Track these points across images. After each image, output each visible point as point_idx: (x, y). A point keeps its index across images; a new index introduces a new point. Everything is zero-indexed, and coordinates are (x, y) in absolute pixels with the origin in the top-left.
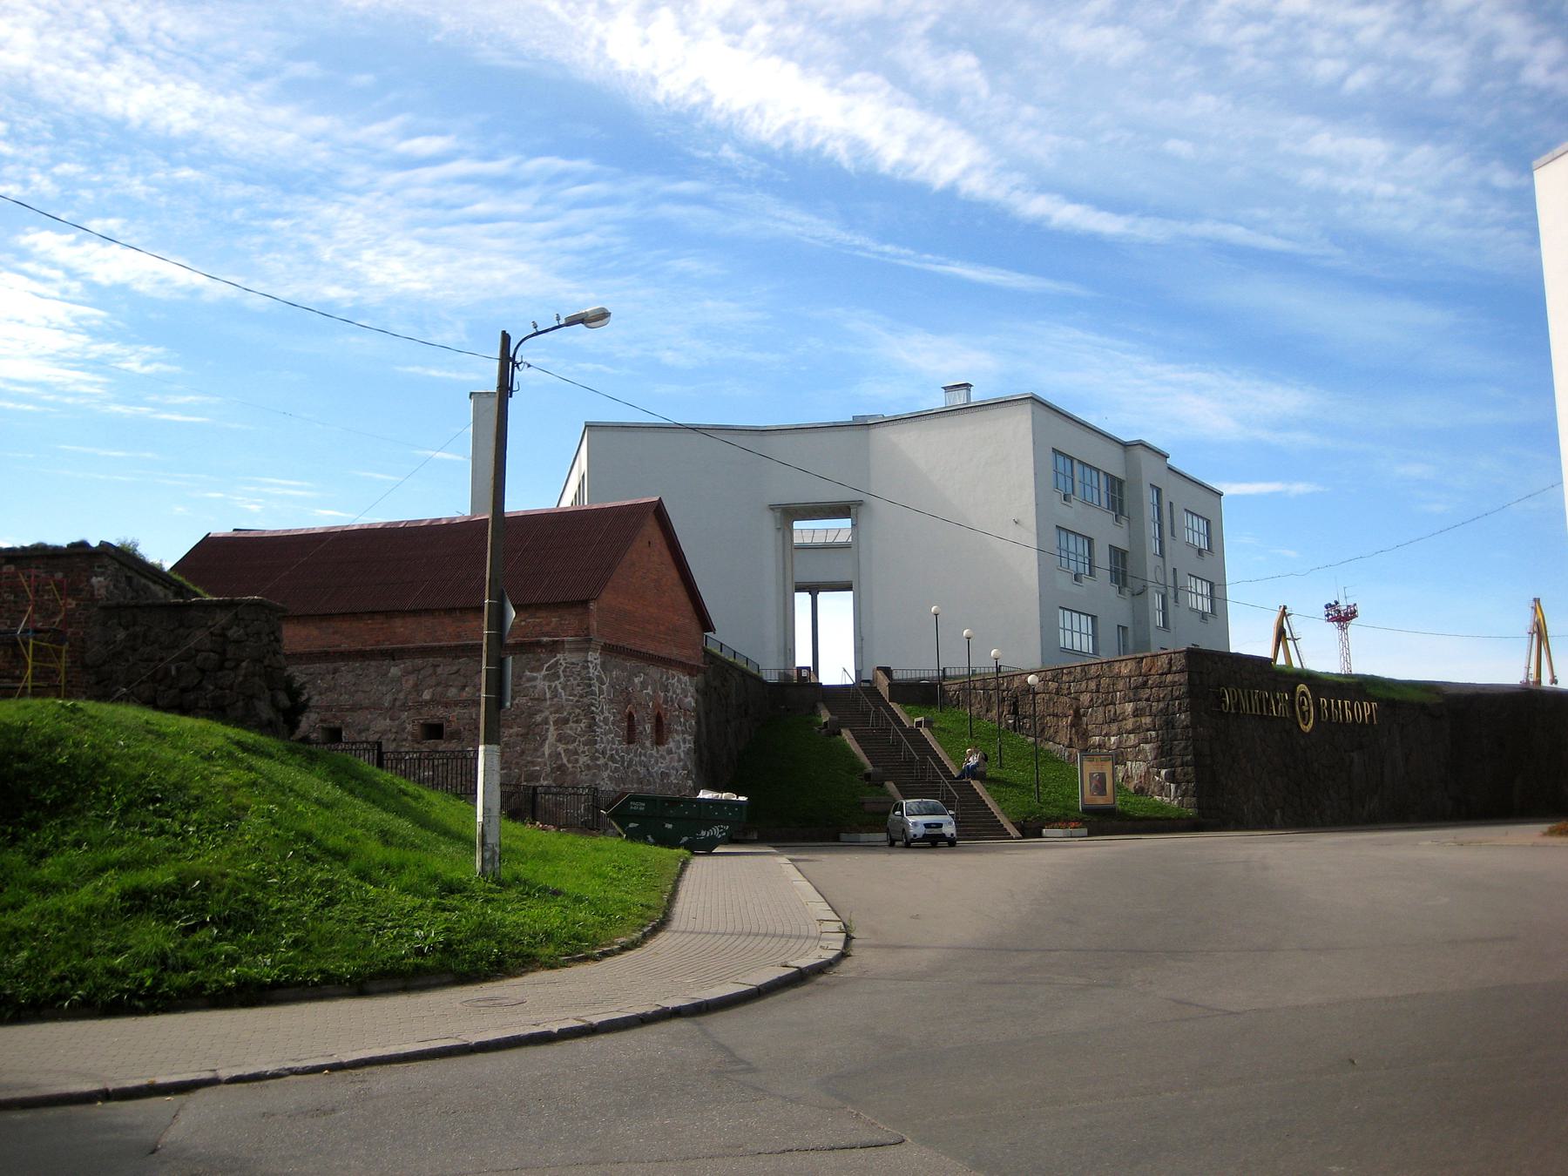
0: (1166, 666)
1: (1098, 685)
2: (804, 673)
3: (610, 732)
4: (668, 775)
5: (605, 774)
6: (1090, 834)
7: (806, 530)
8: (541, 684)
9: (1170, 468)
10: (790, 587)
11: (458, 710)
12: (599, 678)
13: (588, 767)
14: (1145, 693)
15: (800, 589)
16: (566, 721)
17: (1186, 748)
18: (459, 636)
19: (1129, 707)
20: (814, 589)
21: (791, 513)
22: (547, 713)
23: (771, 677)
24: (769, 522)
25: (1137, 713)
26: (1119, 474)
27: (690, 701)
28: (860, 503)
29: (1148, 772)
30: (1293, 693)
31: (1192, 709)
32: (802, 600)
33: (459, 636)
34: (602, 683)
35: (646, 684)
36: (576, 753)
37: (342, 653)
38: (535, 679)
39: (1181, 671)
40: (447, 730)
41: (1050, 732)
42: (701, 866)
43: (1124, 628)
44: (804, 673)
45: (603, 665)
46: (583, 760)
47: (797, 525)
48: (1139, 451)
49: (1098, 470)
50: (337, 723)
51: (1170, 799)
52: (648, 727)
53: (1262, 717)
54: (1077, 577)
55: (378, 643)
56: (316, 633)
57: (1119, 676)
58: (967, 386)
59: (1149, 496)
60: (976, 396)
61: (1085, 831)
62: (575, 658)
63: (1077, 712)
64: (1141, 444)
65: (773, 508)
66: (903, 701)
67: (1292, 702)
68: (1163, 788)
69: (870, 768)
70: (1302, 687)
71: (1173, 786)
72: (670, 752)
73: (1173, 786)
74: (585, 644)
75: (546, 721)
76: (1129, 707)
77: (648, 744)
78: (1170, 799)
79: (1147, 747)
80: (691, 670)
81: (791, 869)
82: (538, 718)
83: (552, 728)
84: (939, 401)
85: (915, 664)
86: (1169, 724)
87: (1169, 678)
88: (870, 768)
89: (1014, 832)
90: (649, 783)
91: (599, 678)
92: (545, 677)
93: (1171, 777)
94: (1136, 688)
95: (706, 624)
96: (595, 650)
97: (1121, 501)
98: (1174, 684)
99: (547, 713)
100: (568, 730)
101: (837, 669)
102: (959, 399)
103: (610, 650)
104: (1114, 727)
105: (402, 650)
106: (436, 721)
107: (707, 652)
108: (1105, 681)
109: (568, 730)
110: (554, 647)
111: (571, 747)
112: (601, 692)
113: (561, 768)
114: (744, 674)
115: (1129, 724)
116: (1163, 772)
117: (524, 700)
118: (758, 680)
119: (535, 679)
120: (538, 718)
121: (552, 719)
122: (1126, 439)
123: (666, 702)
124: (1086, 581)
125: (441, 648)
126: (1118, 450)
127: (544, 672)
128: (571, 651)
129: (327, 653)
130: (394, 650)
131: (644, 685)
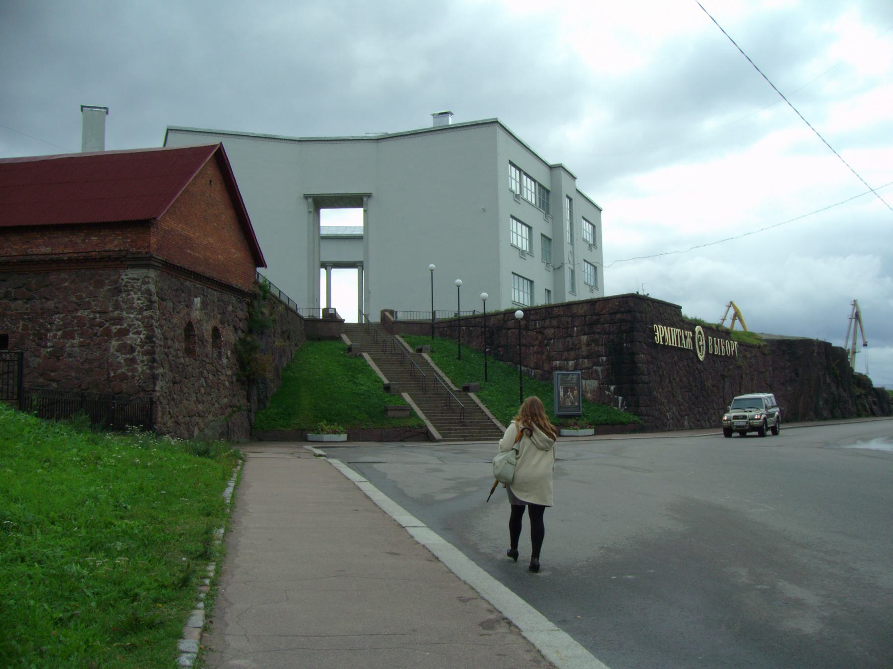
7: (336, 220)
10: (317, 264)
15: (324, 265)
19: (584, 338)
20: (328, 266)
21: (321, 202)
23: (304, 313)
24: (304, 208)
26: (547, 185)
28: (369, 196)
30: (694, 332)
32: (323, 271)
42: (543, 303)
43: (549, 292)
47: (323, 212)
57: (574, 316)
60: (451, 121)
61: (344, 437)
65: (306, 197)
67: (693, 339)
70: (698, 328)
71: (620, 398)
73: (620, 398)
79: (599, 369)
84: (428, 123)
85: (413, 307)
87: (619, 316)
93: (618, 392)
95: (258, 260)
96: (155, 268)
97: (548, 204)
101: (349, 314)
102: (442, 122)
104: (572, 354)
107: (256, 283)
114: (287, 308)
115: (584, 350)
116: (612, 388)
118: (295, 313)
122: (551, 162)
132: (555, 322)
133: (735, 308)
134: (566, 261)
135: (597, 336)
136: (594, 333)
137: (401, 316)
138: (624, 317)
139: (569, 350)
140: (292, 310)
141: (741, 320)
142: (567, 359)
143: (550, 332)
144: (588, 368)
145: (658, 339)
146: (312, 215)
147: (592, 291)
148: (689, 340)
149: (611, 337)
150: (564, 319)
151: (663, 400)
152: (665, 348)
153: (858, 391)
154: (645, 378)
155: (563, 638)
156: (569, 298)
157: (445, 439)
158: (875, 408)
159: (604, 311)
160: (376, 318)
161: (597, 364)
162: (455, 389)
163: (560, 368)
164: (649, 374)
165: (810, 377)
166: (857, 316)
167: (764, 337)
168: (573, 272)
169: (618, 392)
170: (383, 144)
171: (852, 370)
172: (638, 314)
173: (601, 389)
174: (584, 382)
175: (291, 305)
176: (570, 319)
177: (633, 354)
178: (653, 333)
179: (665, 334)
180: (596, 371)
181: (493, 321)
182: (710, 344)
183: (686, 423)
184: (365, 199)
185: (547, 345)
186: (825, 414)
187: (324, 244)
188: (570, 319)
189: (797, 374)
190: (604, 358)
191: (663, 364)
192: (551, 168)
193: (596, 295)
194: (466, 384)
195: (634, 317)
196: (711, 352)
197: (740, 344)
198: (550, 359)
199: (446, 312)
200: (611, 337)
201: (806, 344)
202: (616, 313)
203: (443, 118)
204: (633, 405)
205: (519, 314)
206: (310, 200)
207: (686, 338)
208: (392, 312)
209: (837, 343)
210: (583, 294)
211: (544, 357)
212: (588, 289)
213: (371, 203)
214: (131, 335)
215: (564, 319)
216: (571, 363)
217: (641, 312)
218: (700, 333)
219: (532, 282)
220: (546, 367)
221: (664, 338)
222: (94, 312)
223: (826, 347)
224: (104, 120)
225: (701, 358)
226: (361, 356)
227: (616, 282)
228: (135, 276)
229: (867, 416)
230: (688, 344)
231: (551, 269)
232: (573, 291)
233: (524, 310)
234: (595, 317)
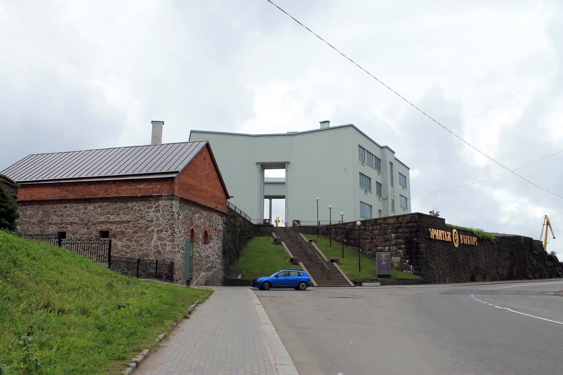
1: (381, 227)
2: (267, 221)
3: (182, 236)
4: (209, 257)
5: (178, 255)
6: (381, 285)
7: (271, 174)
8: (152, 214)
9: (396, 159)
10: (263, 197)
11: (115, 226)
12: (177, 213)
13: (170, 252)
15: (266, 197)
16: (162, 231)
18: (118, 193)
19: (393, 235)
20: (270, 197)
21: (264, 166)
22: (153, 227)
23: (255, 222)
24: (257, 169)
25: (397, 238)
27: (221, 227)
28: (288, 163)
30: (452, 233)
32: (267, 201)
33: (118, 193)
34: (179, 215)
35: (201, 219)
36: (165, 245)
37: (68, 200)
38: (149, 212)
40: (110, 234)
43: (380, 211)
44: (267, 221)
45: (180, 207)
46: (168, 248)
47: (266, 171)
48: (386, 150)
49: (373, 155)
50: (64, 230)
52: (201, 236)
53: (442, 240)
55: (83, 195)
56: (58, 191)
57: (388, 224)
58: (328, 122)
59: (388, 164)
60: (331, 125)
62: (168, 203)
64: (387, 147)
65: (257, 164)
70: (454, 230)
71: (411, 266)
72: (210, 247)
73: (411, 266)
74: (172, 197)
75: (153, 231)
77: (200, 243)
79: (401, 251)
80: (221, 214)
81: (256, 301)
82: (150, 230)
83: (155, 234)
84: (318, 127)
85: (309, 220)
87: (410, 224)
88: (292, 256)
89: (352, 284)
90: (200, 260)
91: (177, 213)
92: (154, 211)
93: (410, 263)
94: (397, 228)
96: (176, 200)
98: (412, 226)
99: (153, 227)
100: (162, 235)
102: (326, 126)
103: (183, 201)
104: (387, 243)
105: (93, 199)
106: (106, 230)
107: (229, 208)
109: (162, 235)
110: (158, 198)
111: (163, 242)
112: (178, 219)
113: (159, 252)
114: (244, 219)
115: (393, 242)
116: (407, 261)
117: (144, 221)
119: (149, 212)
120: (150, 230)
121: (156, 230)
122: (382, 145)
123: (209, 226)
125: (110, 198)
126: (379, 149)
127: (153, 209)
128: (165, 200)
129: (62, 200)
130: (90, 199)
131: (200, 218)
132: (379, 227)
133: (548, 219)
134: (389, 195)
135: (400, 234)
136: (398, 233)
137: (302, 224)
138: (413, 224)
139: (386, 241)
140: (247, 221)
141: (550, 226)
142: (385, 246)
143: (376, 232)
144: (395, 251)
145: (432, 236)
146: (260, 173)
147: (404, 210)
148: (449, 236)
149: (407, 235)
150: (383, 225)
151: (434, 267)
152: (436, 240)
153: (550, 264)
154: (425, 256)
155: (283, 351)
156: (391, 214)
157: (319, 285)
158: (560, 273)
159: (403, 222)
160: (290, 225)
161: (400, 249)
162: (327, 260)
163: (381, 251)
164: (426, 254)
165: (519, 258)
166: (548, 223)
167: (494, 235)
168: (393, 201)
169: (410, 263)
170: (295, 137)
171: (546, 252)
172: (421, 223)
173: (401, 262)
174: (393, 258)
175: (248, 218)
176: (386, 226)
177: (417, 244)
178: (429, 233)
179: (437, 234)
180: (399, 252)
181: (348, 226)
182: (461, 238)
183: (448, 280)
184: (286, 165)
185: (375, 238)
186: (530, 276)
187: (266, 186)
188: (386, 226)
189: (512, 255)
190: (403, 246)
191: (434, 249)
192: (382, 148)
193: (406, 213)
194: (332, 258)
195: (421, 226)
196: (462, 242)
197: (478, 239)
198: (376, 246)
199: (325, 221)
200: (407, 235)
201: (516, 239)
202: (409, 223)
203: (327, 124)
204: (417, 271)
205: (359, 223)
206: (259, 165)
207: (447, 235)
208: (298, 222)
209: (535, 238)
210: (399, 212)
211: (373, 245)
212: (402, 209)
213: (290, 167)
214: (164, 232)
215: (383, 225)
216: (387, 248)
217: (422, 222)
218: (455, 233)
219: (371, 206)
220: (374, 250)
221: (435, 236)
222: (147, 221)
223: (529, 242)
224: (162, 128)
225: (456, 246)
226: (281, 244)
227: (418, 206)
228: (166, 204)
229: (556, 277)
230: (449, 239)
231: (382, 199)
232: (393, 210)
233: (361, 221)
234: (399, 225)
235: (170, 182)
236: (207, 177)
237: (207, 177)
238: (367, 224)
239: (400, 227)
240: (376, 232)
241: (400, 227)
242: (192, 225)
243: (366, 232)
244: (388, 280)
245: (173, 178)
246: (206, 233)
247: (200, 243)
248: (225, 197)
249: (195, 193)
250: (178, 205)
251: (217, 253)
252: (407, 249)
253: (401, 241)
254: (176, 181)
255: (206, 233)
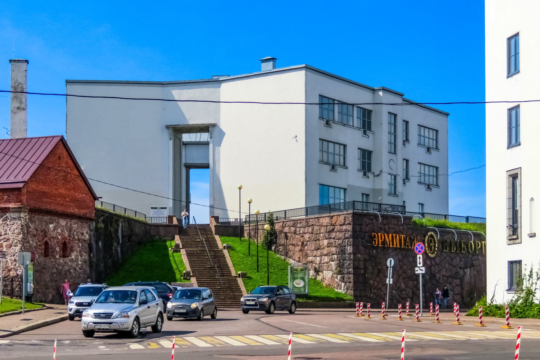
0: (343, 221)
1: (313, 230)
7: (186, 137)
14: (333, 235)
17: (349, 264)
19: (326, 242)
25: (329, 245)
28: (214, 125)
29: (332, 276)
31: (354, 245)
35: (57, 229)
39: (349, 224)
41: (291, 253)
51: (342, 290)
54: (429, 149)
57: (321, 226)
63: (303, 243)
65: (168, 127)
66: (221, 235)
68: (338, 285)
69: (81, 286)
71: (343, 284)
73: (343, 284)
76: (326, 242)
77: (57, 257)
78: (342, 290)
86: (342, 252)
87: (344, 227)
93: (343, 279)
94: (329, 232)
96: (25, 212)
98: (346, 230)
104: (319, 252)
108: (316, 228)
124: (433, 152)
128: (13, 212)
131: (55, 228)
136: (330, 238)
190: (336, 256)
228: (14, 217)
234: (332, 227)
235: (17, 193)
236: (64, 179)
237: (64, 179)
238: (298, 225)
239: (333, 230)
240: (307, 236)
241: (333, 230)
242: (46, 237)
243: (297, 236)
244: (342, 303)
245: (19, 189)
246: (65, 244)
247: (57, 257)
248: (92, 198)
249: (48, 200)
250: (27, 217)
251: (82, 266)
252: (340, 260)
253: (333, 249)
254: (24, 191)
255: (65, 244)
